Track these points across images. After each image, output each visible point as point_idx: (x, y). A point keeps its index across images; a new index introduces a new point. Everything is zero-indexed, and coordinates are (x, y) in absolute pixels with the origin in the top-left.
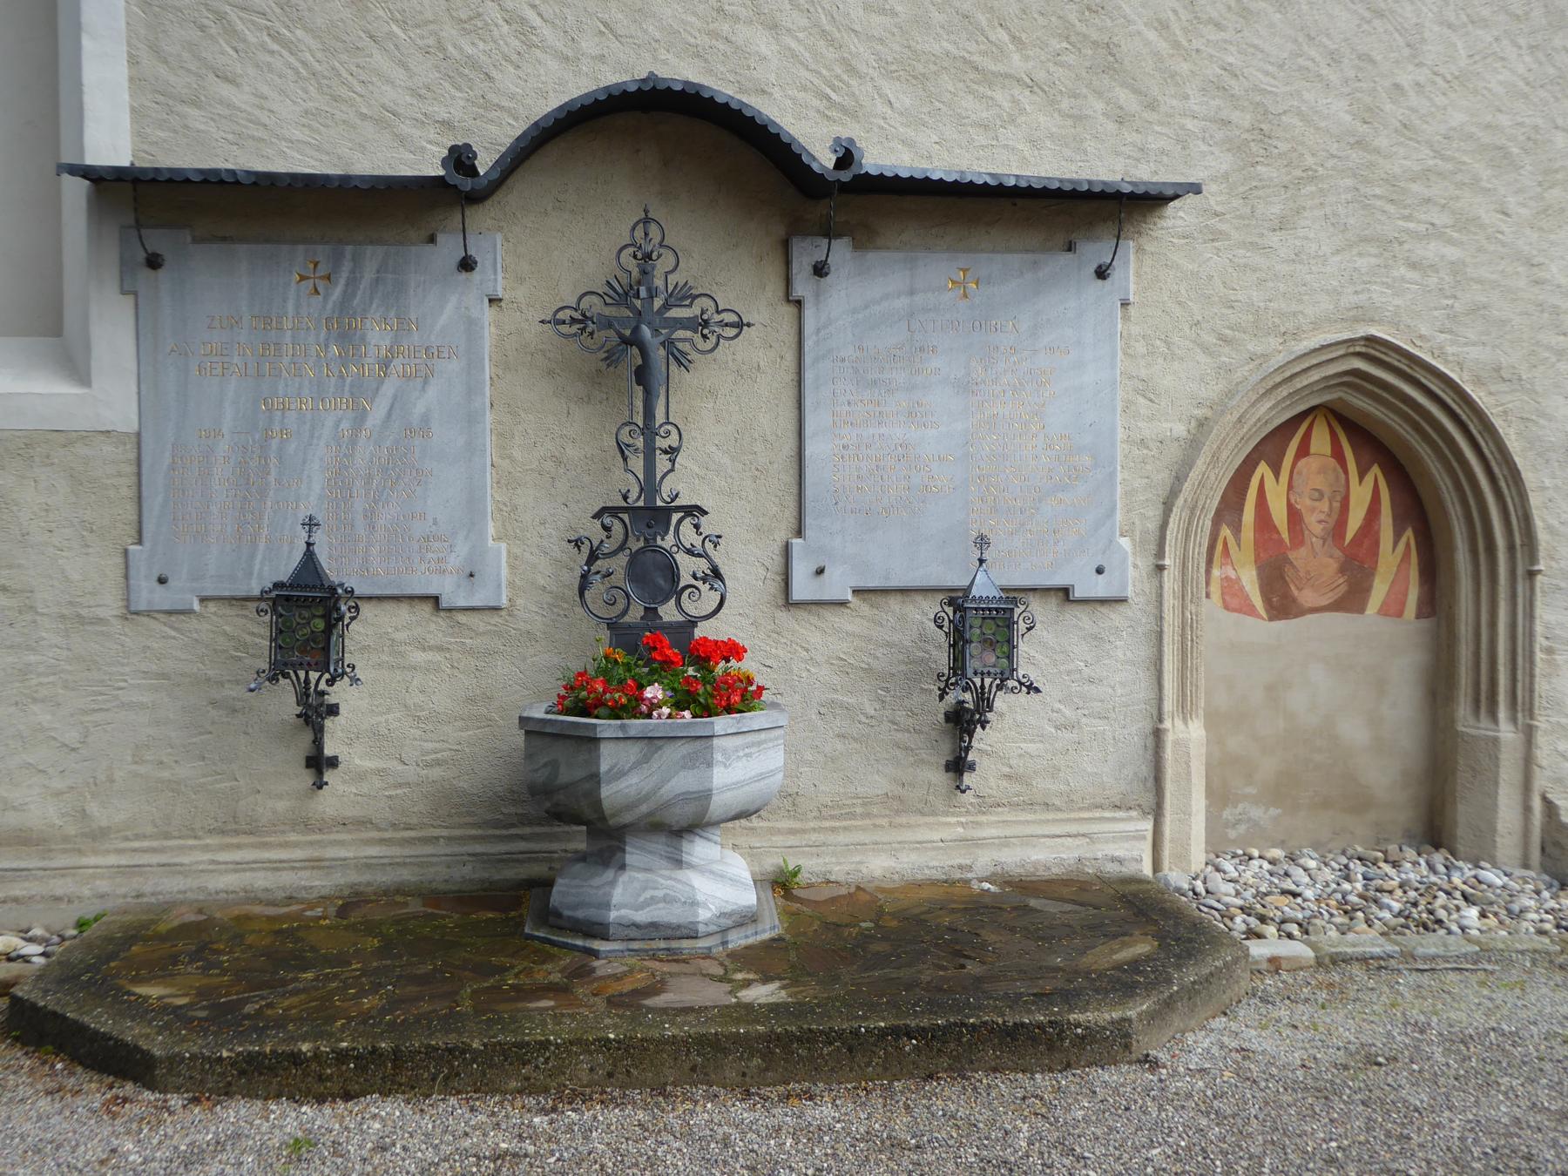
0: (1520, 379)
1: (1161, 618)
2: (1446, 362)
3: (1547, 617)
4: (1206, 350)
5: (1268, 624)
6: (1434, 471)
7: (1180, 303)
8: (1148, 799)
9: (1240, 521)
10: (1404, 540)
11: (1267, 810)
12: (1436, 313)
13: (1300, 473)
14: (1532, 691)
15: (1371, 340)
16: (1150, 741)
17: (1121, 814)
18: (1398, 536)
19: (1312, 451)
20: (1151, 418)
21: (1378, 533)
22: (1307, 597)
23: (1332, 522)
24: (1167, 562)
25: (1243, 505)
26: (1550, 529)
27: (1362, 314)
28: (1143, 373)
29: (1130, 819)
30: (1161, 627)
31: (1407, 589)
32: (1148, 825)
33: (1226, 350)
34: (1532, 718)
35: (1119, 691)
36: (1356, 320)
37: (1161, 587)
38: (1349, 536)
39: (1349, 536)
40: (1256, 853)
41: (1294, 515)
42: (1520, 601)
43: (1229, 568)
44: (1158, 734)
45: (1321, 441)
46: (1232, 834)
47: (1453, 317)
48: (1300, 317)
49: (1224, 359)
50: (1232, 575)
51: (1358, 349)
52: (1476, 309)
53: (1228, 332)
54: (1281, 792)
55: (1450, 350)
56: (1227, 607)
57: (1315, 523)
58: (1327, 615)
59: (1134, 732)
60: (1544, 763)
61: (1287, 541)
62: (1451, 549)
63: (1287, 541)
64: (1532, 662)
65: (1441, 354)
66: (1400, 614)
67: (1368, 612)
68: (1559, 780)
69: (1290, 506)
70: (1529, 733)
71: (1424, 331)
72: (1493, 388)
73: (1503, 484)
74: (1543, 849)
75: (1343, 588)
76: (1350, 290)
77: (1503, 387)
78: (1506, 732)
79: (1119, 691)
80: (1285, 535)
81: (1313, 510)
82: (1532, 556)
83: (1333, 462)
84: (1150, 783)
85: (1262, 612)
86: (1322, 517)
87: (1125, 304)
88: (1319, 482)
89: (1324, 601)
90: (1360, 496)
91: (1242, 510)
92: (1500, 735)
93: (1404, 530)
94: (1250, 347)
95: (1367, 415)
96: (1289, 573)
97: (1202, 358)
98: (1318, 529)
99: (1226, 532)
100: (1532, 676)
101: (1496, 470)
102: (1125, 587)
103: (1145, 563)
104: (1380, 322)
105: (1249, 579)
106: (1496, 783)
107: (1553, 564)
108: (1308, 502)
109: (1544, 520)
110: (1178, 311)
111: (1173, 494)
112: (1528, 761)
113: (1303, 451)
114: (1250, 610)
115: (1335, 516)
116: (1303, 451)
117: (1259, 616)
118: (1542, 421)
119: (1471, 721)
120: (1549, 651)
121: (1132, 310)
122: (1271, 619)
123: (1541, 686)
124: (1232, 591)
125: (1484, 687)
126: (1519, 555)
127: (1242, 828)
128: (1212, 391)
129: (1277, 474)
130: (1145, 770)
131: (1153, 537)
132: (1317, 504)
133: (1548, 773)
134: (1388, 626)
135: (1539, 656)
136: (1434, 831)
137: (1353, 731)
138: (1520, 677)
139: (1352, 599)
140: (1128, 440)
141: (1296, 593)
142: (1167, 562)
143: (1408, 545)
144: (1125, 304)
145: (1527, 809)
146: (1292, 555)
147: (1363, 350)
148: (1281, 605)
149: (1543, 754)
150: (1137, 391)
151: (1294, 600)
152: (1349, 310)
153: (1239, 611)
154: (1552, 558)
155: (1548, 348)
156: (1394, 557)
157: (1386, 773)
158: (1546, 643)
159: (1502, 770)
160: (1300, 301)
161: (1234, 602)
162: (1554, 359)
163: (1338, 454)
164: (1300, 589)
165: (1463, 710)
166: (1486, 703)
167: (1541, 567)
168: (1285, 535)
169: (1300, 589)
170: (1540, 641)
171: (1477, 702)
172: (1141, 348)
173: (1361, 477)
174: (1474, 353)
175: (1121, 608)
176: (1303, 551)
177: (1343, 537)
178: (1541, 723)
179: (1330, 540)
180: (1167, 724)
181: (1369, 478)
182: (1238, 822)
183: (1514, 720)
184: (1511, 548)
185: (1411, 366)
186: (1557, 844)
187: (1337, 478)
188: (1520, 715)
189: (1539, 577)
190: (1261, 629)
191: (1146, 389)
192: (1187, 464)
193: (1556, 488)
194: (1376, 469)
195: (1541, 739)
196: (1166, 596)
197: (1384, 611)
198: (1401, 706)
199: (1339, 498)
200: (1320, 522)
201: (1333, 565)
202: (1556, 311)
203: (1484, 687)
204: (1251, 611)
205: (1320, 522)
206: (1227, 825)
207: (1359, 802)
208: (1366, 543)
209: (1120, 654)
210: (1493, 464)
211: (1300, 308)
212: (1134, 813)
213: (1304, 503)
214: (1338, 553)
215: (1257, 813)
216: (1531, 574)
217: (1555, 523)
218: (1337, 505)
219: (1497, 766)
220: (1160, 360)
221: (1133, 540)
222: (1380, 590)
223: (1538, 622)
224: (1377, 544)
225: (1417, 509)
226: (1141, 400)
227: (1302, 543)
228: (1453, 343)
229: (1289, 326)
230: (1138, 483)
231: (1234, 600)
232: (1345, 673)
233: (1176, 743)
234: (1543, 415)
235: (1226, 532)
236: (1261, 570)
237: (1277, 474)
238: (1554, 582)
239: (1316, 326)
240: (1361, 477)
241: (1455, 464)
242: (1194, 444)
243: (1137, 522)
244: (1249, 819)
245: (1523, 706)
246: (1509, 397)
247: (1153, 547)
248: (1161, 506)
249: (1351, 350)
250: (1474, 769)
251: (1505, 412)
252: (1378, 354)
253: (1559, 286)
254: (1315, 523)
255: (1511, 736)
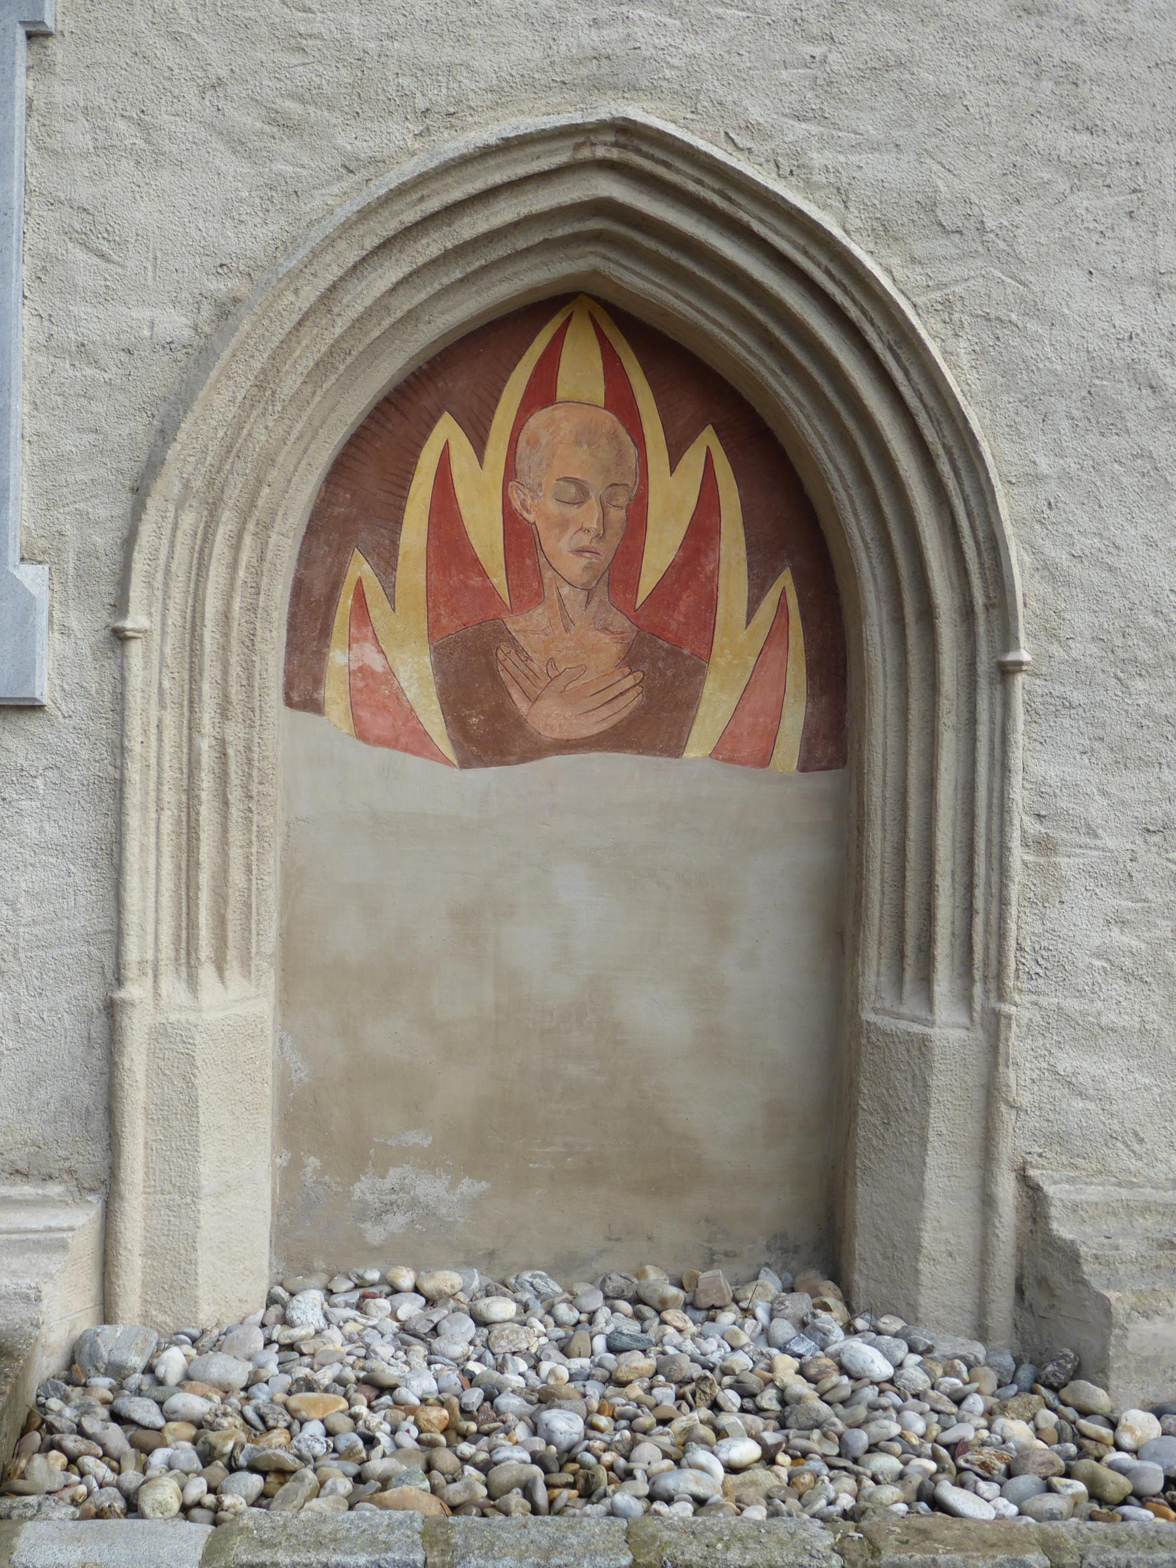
0: (982, 229)
1: (123, 750)
2: (809, 186)
3: (1039, 769)
4: (237, 144)
5: (457, 771)
6: (813, 439)
7: (175, 37)
8: (89, 1159)
9: (395, 545)
10: (773, 595)
11: (453, 1186)
12: (785, 75)
13: (533, 443)
14: (1002, 936)
15: (627, 131)
16: (98, 1028)
17: (27, 1190)
18: (758, 588)
19: (561, 393)
20: (104, 297)
21: (713, 577)
22: (549, 716)
23: (607, 550)
24: (134, 621)
25: (402, 509)
26: (1048, 570)
27: (604, 71)
28: (84, 193)
29: (44, 1202)
30: (121, 768)
31: (780, 704)
32: (82, 1219)
33: (288, 146)
34: (1001, 997)
35: (27, 913)
36: (596, 85)
37: (123, 680)
38: (648, 581)
39: (648, 581)
40: (406, 1279)
41: (519, 535)
42: (983, 730)
43: (369, 649)
44: (112, 1010)
45: (581, 370)
46: (375, 1234)
47: (828, 86)
48: (463, 76)
49: (279, 166)
50: (377, 663)
51: (601, 152)
52: (880, 69)
53: (290, 105)
54: (487, 1142)
55: (817, 159)
56: (362, 735)
57: (569, 551)
58: (595, 756)
59: (63, 1008)
60: (1025, 1099)
61: (503, 591)
62: (859, 615)
63: (503, 591)
64: (1004, 871)
65: (798, 170)
66: (764, 760)
67: (690, 753)
68: (1060, 1139)
69: (510, 515)
70: (994, 1027)
71: (756, 114)
72: (919, 248)
73: (944, 467)
74: (1020, 1290)
75: (632, 701)
76: (582, 16)
77: (943, 246)
78: (948, 1027)
79: (27, 913)
80: (499, 579)
81: (563, 524)
82: (1007, 636)
83: (609, 420)
84: (97, 1123)
85: (445, 747)
86: (585, 540)
87: (36, 35)
88: (579, 462)
89: (591, 727)
90: (672, 495)
91: (399, 522)
92: (935, 1032)
93: (775, 574)
94: (341, 141)
95: (666, 313)
96: (507, 662)
97: (230, 164)
98: (575, 567)
99: (360, 568)
100: (1003, 902)
101: (930, 434)
102: (26, 673)
103: (84, 625)
104: (653, 91)
105: (415, 675)
106: (923, 1141)
107: (1055, 649)
108: (553, 507)
109: (1035, 550)
110: (169, 54)
111: (153, 467)
112: (991, 1094)
113: (542, 392)
114: (417, 742)
115: (614, 540)
116: (542, 392)
117: (437, 756)
118: (1032, 326)
119: (888, 1002)
120: (1044, 846)
121: (57, 50)
122: (465, 764)
123: (1022, 924)
124: (374, 696)
125: (912, 924)
126: (981, 629)
127: (397, 1221)
128: (255, 236)
129: (479, 443)
130: (87, 1093)
131: (106, 567)
132: (573, 511)
133: (1033, 1122)
134: (737, 786)
135: (1018, 855)
136: (825, 1247)
137: (656, 1014)
138: (979, 903)
139: (654, 723)
140: (48, 345)
141: (523, 707)
142: (134, 621)
143: (782, 605)
144: (36, 35)
145: (987, 1202)
146: (514, 624)
147: (615, 154)
148: (488, 729)
149: (1021, 1078)
150: (68, 233)
151: (519, 723)
152: (579, 62)
153: (391, 743)
154: (1053, 636)
155: (1051, 159)
156: (748, 633)
157: (729, 1114)
158: (1034, 828)
159: (933, 1112)
160: (463, 40)
161: (380, 725)
162: (1063, 185)
163: (620, 401)
164: (533, 700)
165: (874, 972)
166: (915, 963)
167: (1025, 656)
168: (499, 579)
169: (533, 700)
170: (1021, 823)
171: (900, 954)
172: (78, 135)
173: (674, 462)
174: (875, 167)
175: (31, 724)
176: (539, 616)
177: (632, 585)
178: (1020, 1009)
179: (602, 594)
180: (135, 991)
181: (694, 459)
182: (389, 1208)
183: (967, 999)
184: (967, 613)
185: (730, 197)
186: (1043, 1282)
187: (620, 455)
188: (978, 989)
189: (1020, 679)
190: (442, 785)
191: (92, 231)
192: (182, 400)
193: (1065, 477)
194: (708, 438)
195: (1016, 1044)
196: (135, 700)
197: (726, 751)
198: (765, 964)
199: (623, 500)
200: (580, 551)
201: (611, 649)
202: (1070, 76)
203: (912, 924)
204: (420, 744)
205: (580, 551)
206: (363, 1213)
207: (667, 1169)
208: (687, 600)
209: (30, 828)
210: (922, 419)
211: (462, 55)
212: (55, 1190)
213: (541, 510)
214: (621, 622)
215: (431, 1188)
216: (1006, 672)
217: (1060, 556)
218: (617, 515)
219: (926, 1102)
220: (127, 166)
221: (56, 570)
222: (716, 706)
223: (1017, 779)
224: (711, 602)
225: (798, 533)
226: (79, 254)
227: (538, 597)
228: (825, 143)
229: (438, 95)
230: (72, 443)
231: (381, 719)
232: (625, 884)
233: (160, 1033)
234: (1034, 310)
235: (360, 568)
236: (442, 654)
237: (479, 443)
238: (1058, 690)
239: (501, 95)
240: (674, 462)
241: (850, 423)
242: (199, 357)
243: (69, 530)
244: (414, 1203)
245: (985, 971)
246: (957, 271)
247: (106, 590)
248: (126, 497)
249: (585, 153)
250: (886, 1108)
251: (947, 304)
252: (648, 165)
253: (1080, 20)
254: (569, 551)
255: (957, 1035)
